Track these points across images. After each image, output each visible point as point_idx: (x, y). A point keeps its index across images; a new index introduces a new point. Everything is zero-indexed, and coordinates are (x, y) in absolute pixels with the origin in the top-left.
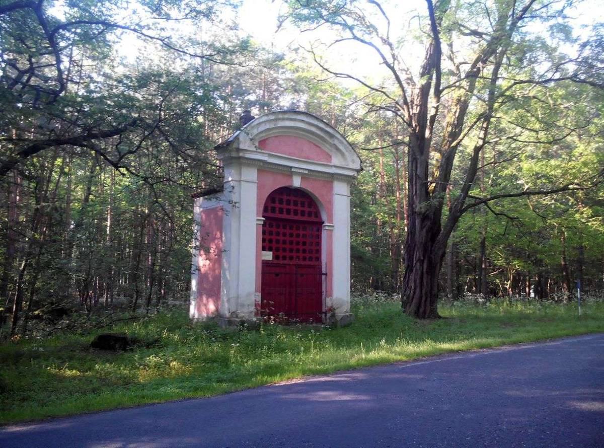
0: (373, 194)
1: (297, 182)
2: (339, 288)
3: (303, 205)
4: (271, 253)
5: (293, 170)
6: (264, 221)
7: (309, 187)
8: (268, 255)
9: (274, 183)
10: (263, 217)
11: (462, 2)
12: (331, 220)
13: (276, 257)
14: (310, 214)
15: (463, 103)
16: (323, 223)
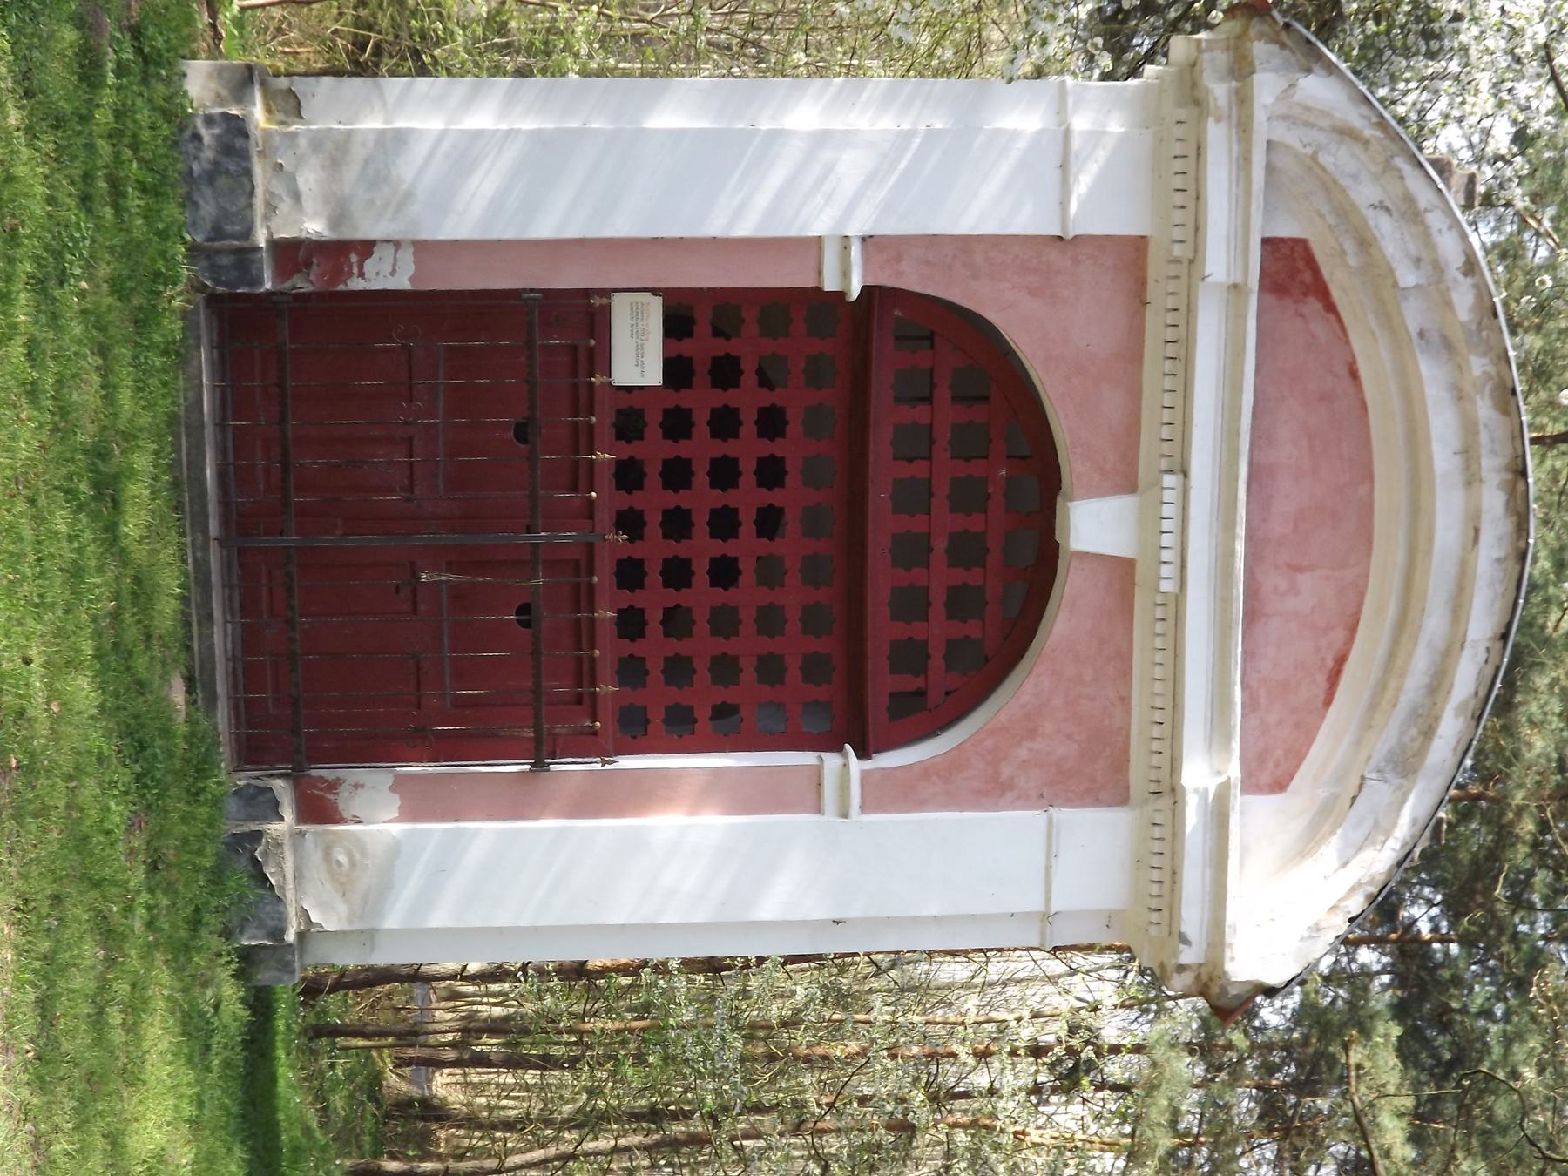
0: (1052, 1066)
1: (1092, 525)
2: (456, 874)
3: (961, 603)
4: (653, 376)
5: (1169, 480)
6: (840, 295)
7: (1067, 620)
8: (640, 364)
9: (1049, 340)
10: (865, 290)
11: (1126, 5)
12: (886, 795)
13: (630, 410)
14: (909, 657)
15: (1373, 1016)
16: (863, 754)
